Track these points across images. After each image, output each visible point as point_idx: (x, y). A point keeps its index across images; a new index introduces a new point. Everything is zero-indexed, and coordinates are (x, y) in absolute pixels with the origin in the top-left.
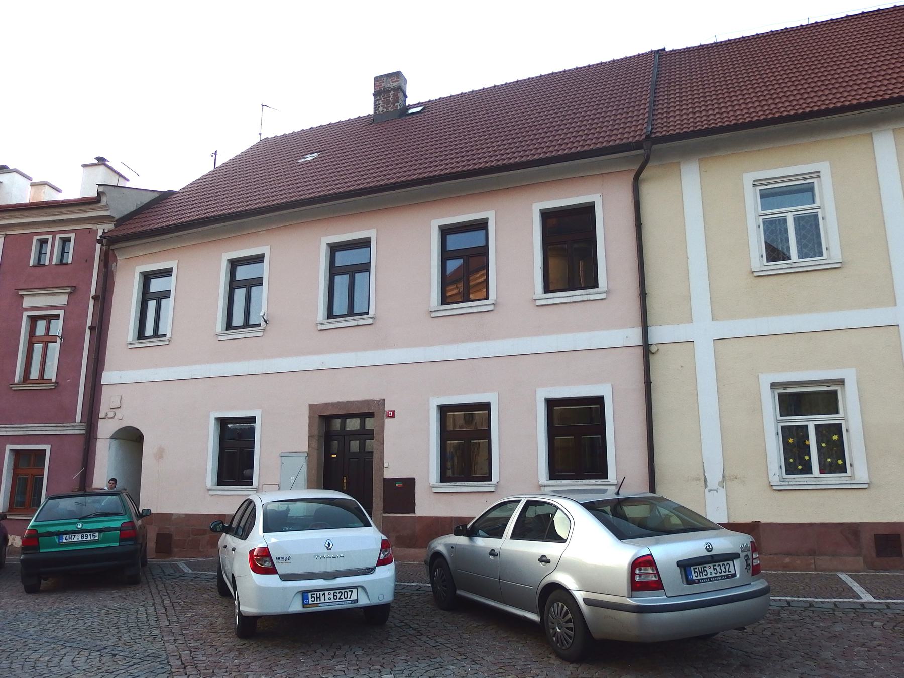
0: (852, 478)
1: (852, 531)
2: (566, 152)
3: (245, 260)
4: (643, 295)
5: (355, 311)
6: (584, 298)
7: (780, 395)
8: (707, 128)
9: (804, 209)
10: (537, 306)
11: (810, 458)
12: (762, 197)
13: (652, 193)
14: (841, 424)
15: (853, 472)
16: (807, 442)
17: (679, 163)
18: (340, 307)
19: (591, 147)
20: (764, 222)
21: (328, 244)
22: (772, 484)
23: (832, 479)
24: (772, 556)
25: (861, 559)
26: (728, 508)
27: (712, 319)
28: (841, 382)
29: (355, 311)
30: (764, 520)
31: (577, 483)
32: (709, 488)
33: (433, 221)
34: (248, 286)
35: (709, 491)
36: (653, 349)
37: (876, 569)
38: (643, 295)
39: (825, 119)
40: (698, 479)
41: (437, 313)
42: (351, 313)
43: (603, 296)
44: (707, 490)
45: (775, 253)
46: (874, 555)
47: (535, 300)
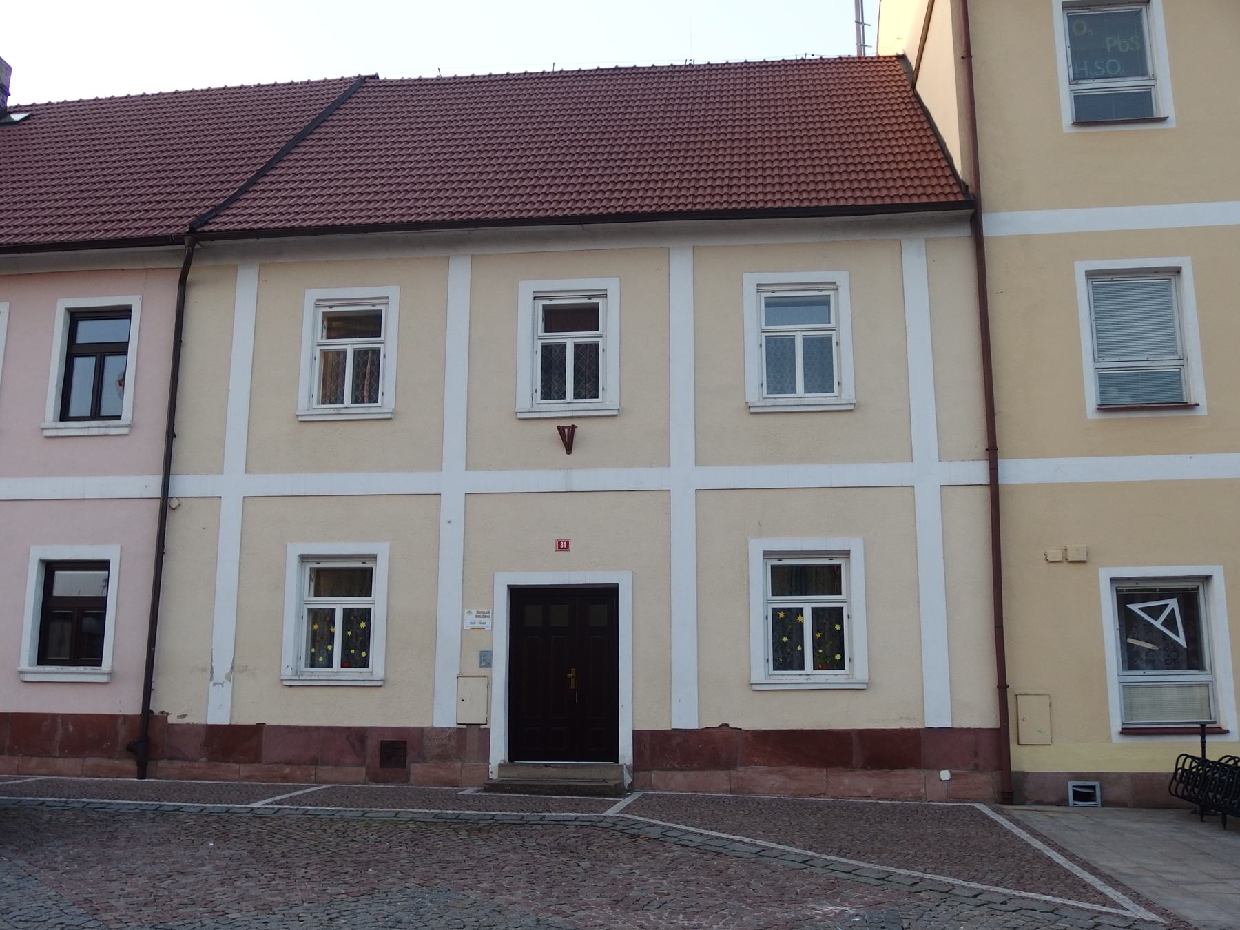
0: (850, 677)
1: (357, 736)
2: (530, 214)
3: (89, 312)
4: (171, 435)
5: (103, 413)
6: (102, 431)
7: (773, 567)
8: (762, 208)
9: (816, 329)
10: (46, 437)
11: (333, 648)
12: (767, 305)
13: (201, 302)
14: (842, 608)
15: (852, 669)
16: (332, 630)
17: (236, 267)
18: (81, 402)
19: (548, 213)
20: (766, 340)
21: (68, 310)
22: (282, 678)
23: (353, 673)
24: (271, 765)
25: (364, 770)
26: (232, 706)
27: (246, 470)
28: (846, 554)
29: (103, 413)
30: (269, 722)
31: (62, 671)
32: (214, 681)
33: (521, 283)
34: (99, 355)
35: (215, 684)
36: (174, 503)
37: (378, 782)
38: (171, 435)
39: (399, 234)
40: (204, 670)
41: (63, 430)
42: (96, 414)
43: (125, 431)
44: (211, 684)
45: (331, 393)
46: (378, 765)
47: (43, 429)
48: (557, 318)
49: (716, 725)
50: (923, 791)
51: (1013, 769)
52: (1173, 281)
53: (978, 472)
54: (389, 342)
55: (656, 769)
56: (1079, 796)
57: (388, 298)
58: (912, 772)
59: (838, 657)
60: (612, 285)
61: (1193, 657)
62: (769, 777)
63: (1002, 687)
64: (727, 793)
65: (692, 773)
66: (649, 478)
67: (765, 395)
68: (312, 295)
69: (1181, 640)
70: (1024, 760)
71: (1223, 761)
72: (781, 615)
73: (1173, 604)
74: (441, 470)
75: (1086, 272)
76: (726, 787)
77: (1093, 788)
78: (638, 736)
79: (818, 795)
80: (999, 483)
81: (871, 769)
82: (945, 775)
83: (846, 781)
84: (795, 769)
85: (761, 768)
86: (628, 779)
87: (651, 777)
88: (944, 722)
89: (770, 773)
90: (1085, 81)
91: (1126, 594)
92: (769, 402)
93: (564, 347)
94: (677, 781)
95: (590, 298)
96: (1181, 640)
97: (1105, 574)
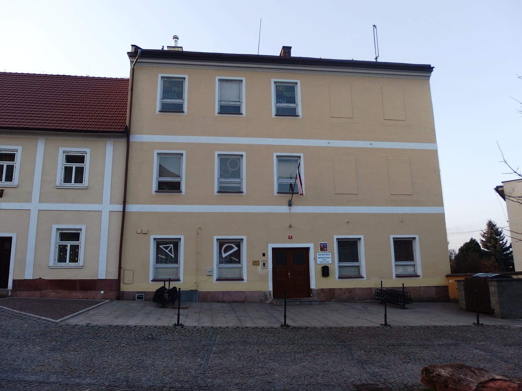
23: (73, 264)
28: (81, 230)
48: (70, 159)
49: (38, 278)
50: (96, 297)
51: (121, 290)
52: (299, 159)
53: (120, 208)
54: (87, 165)
55: (19, 291)
56: (138, 298)
57: (18, 150)
58: (93, 291)
59: (76, 259)
60: (20, 148)
61: (176, 260)
62: (52, 293)
63: (120, 268)
64: (39, 297)
65: (29, 292)
66: (25, 206)
67: (62, 183)
68: (61, 150)
69: (173, 256)
70: (125, 288)
71: (387, 290)
72: (61, 247)
73: (172, 246)
74: (31, 203)
75: (157, 153)
76: (39, 296)
77: (143, 295)
78: (14, 281)
79: (66, 298)
80: (126, 211)
81: (82, 291)
82: (102, 292)
83: (74, 294)
84: (60, 291)
85: (50, 290)
86: (10, 294)
87: (17, 293)
88: (104, 278)
89: (52, 292)
90: (165, 99)
91: (159, 242)
92: (63, 185)
93: (3, 166)
94: (25, 294)
95: (13, 152)
96: (173, 256)
97: (152, 237)
